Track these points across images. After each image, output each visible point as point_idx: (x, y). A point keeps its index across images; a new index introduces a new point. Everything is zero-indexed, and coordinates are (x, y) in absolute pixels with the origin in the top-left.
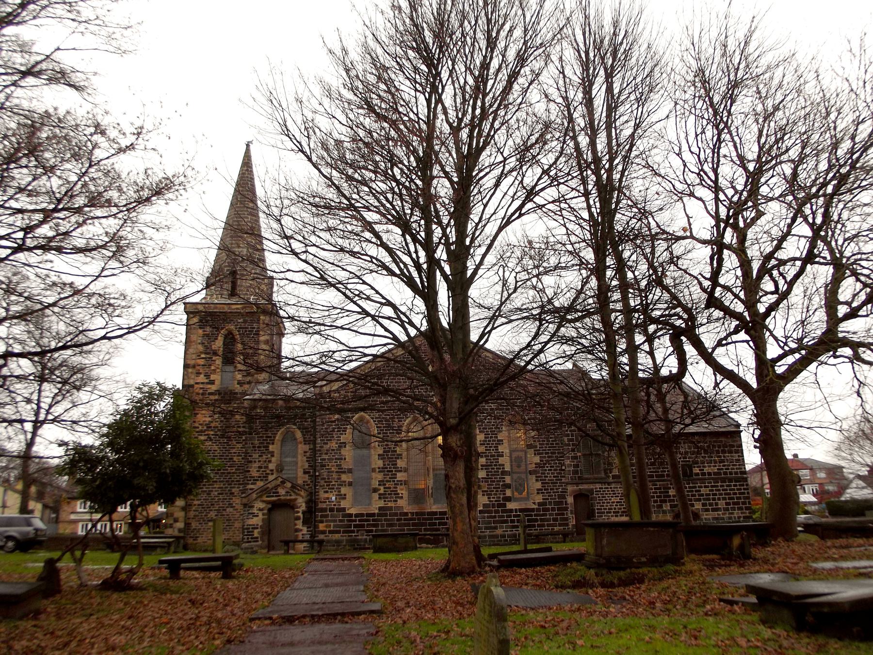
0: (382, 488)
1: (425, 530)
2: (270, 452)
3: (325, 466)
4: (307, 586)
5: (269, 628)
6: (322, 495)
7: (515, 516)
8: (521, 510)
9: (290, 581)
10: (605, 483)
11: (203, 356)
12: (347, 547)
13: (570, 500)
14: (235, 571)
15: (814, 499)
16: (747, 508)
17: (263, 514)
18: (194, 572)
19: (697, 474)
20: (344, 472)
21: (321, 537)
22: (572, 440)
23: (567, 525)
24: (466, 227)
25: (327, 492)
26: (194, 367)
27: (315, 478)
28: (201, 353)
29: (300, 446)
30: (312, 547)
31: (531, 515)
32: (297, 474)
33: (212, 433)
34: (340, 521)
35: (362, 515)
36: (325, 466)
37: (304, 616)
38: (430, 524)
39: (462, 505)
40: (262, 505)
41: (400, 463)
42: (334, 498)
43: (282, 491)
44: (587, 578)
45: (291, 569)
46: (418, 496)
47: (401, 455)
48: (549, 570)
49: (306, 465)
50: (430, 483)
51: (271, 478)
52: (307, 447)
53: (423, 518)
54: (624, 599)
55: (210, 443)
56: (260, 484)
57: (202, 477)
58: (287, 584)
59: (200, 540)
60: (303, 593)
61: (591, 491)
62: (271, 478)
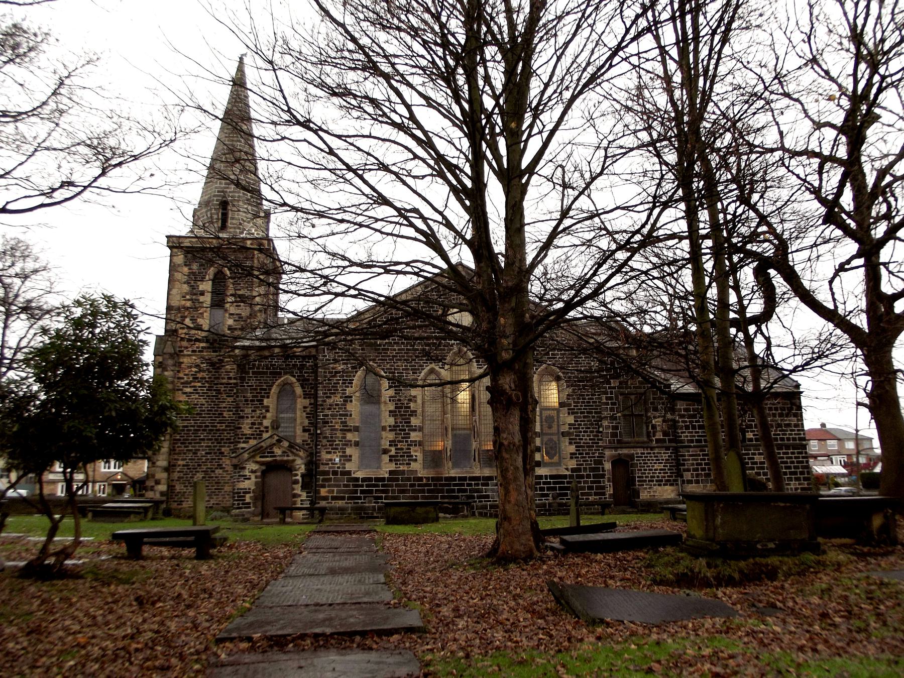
0: (393, 449)
1: (442, 497)
2: (263, 407)
3: (327, 423)
4: (306, 571)
5: (247, 658)
6: (325, 456)
7: (544, 483)
8: (552, 477)
9: (284, 562)
10: (647, 448)
11: (188, 297)
12: (353, 516)
13: (608, 466)
14: (215, 547)
15: (844, 471)
16: (805, 479)
17: (256, 477)
18: (163, 549)
19: (751, 440)
20: (350, 430)
21: (323, 504)
22: (611, 398)
23: (604, 494)
24: (527, 88)
25: (329, 453)
26: (178, 309)
27: (315, 437)
28: (187, 294)
29: (299, 400)
30: (312, 515)
31: (563, 483)
32: (295, 432)
33: (199, 384)
34: (345, 486)
35: (370, 479)
36: (327, 423)
37: (303, 637)
38: (448, 491)
39: (517, 468)
40: (255, 467)
41: (414, 421)
42: (337, 460)
43: (278, 451)
44: (697, 570)
45: (286, 545)
46: (435, 459)
47: (416, 411)
48: (638, 558)
49: (306, 422)
50: (449, 444)
51: (265, 435)
52: (307, 402)
53: (439, 484)
54: (773, 606)
55: (197, 396)
56: (253, 442)
57: (165, 425)
58: (280, 570)
59: (185, 505)
60: (299, 583)
61: (632, 457)
62: (265, 435)
